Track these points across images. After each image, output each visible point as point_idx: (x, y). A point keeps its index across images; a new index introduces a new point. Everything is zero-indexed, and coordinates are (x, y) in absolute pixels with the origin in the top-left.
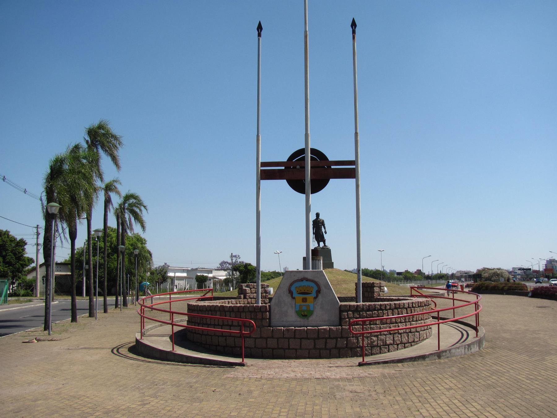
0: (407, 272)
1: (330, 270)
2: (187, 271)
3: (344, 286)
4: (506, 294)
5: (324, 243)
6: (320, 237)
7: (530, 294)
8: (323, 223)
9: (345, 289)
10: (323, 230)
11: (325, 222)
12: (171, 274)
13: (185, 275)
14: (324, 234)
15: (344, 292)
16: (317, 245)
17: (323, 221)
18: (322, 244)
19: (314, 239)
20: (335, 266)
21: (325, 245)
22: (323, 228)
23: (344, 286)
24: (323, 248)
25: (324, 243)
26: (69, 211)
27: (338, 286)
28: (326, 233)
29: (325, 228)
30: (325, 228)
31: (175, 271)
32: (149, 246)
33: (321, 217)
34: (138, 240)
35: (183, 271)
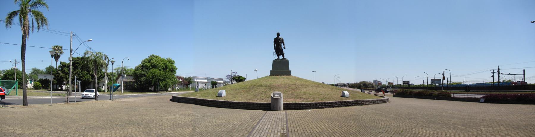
0: (38, 70)
1: (288, 76)
2: (208, 79)
3: (303, 90)
4: (437, 99)
5: (283, 57)
6: (279, 50)
7: (483, 100)
8: (282, 41)
9: (305, 93)
10: (283, 46)
11: (284, 41)
12: (198, 80)
13: (206, 81)
15: (304, 96)
16: (277, 57)
17: (283, 40)
18: (281, 57)
20: (292, 74)
21: (284, 58)
23: (303, 90)
24: (282, 60)
25: (283, 57)
26: (63, 73)
27: (297, 90)
28: (285, 48)
29: (284, 44)
30: (284, 44)
31: (199, 79)
32: (176, 65)
33: (281, 36)
34: (169, 62)
35: (205, 79)
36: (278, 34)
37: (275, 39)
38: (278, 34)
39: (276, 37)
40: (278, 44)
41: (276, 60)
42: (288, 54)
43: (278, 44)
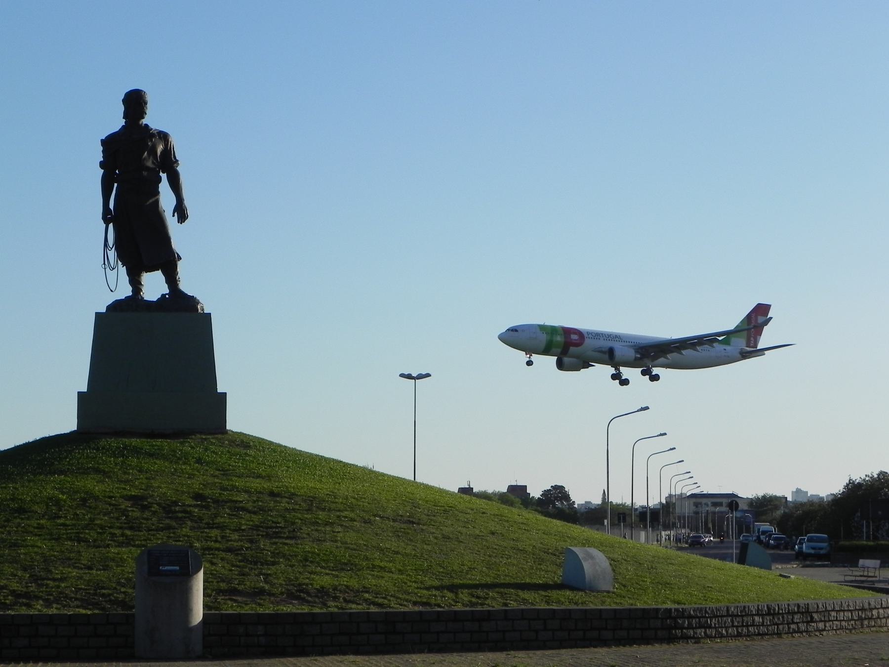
6: (139, 236)
10: (166, 199)
11: (180, 153)
14: (171, 221)
19: (112, 254)
22: (164, 187)
25: (172, 279)
28: (181, 213)
33: (153, 119)
36: (135, 103)
37: (109, 143)
38: (135, 103)
39: (116, 122)
40: (136, 173)
41: (116, 307)
42: (206, 261)
43: (136, 173)
